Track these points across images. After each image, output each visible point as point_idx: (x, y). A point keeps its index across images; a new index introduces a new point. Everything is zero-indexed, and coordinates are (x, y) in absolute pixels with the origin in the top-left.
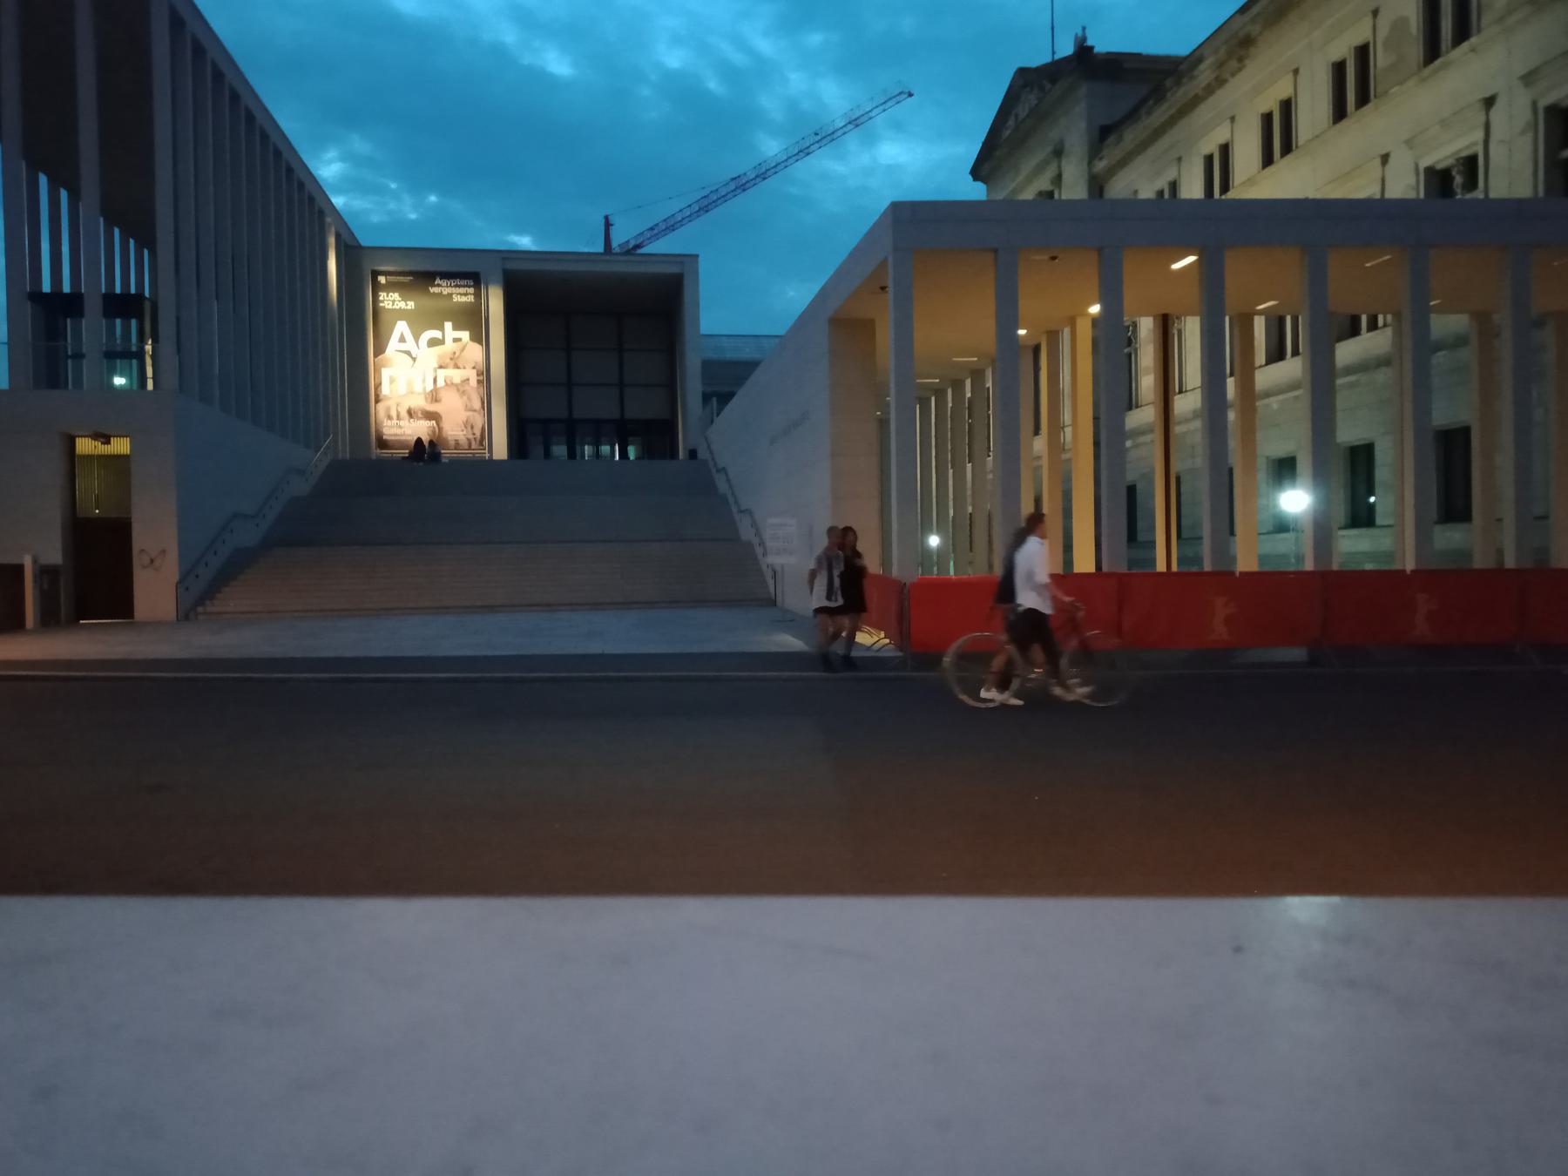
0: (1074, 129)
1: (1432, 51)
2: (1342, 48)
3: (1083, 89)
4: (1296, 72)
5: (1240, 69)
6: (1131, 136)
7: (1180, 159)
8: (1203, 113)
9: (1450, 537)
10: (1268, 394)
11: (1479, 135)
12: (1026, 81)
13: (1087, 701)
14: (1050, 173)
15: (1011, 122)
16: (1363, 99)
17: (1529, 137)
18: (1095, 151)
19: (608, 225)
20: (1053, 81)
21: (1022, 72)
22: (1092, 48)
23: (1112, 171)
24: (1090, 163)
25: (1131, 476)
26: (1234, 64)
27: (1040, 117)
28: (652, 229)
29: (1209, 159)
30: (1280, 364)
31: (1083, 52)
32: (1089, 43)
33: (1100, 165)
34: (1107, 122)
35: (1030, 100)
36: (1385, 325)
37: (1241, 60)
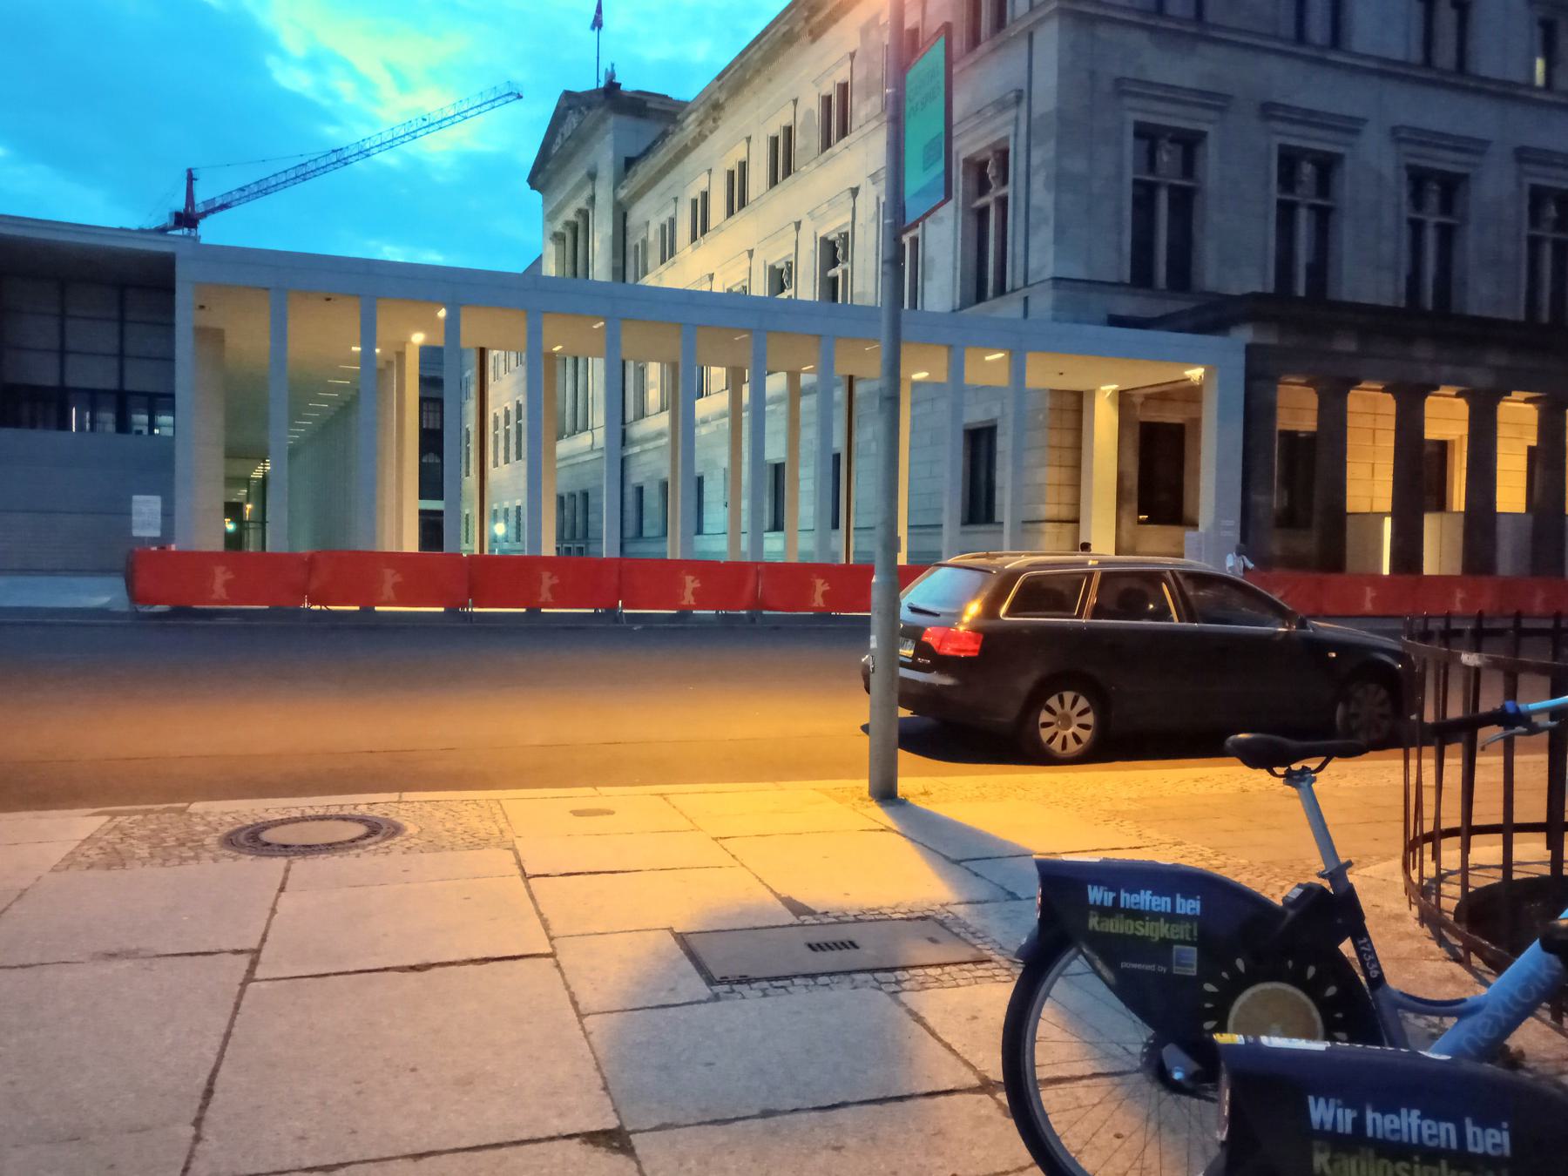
0: (603, 154)
1: (827, 144)
2: (775, 129)
3: (612, 120)
4: (749, 139)
5: (716, 128)
6: (643, 171)
7: (676, 199)
8: (692, 161)
9: (838, 541)
10: (705, 422)
11: (849, 218)
12: (571, 102)
13: (1468, 1066)
14: (587, 193)
15: (559, 140)
16: (788, 172)
17: (874, 225)
18: (618, 183)
19: (191, 179)
20: (589, 108)
21: (567, 95)
22: (619, 85)
23: (638, 195)
24: (615, 189)
25: (698, 470)
26: (710, 123)
27: (581, 139)
28: (242, 189)
29: (694, 202)
30: (982, 305)
31: (612, 88)
32: (617, 80)
33: (622, 194)
34: (632, 153)
35: (573, 120)
36: (1013, 290)
37: (715, 120)
